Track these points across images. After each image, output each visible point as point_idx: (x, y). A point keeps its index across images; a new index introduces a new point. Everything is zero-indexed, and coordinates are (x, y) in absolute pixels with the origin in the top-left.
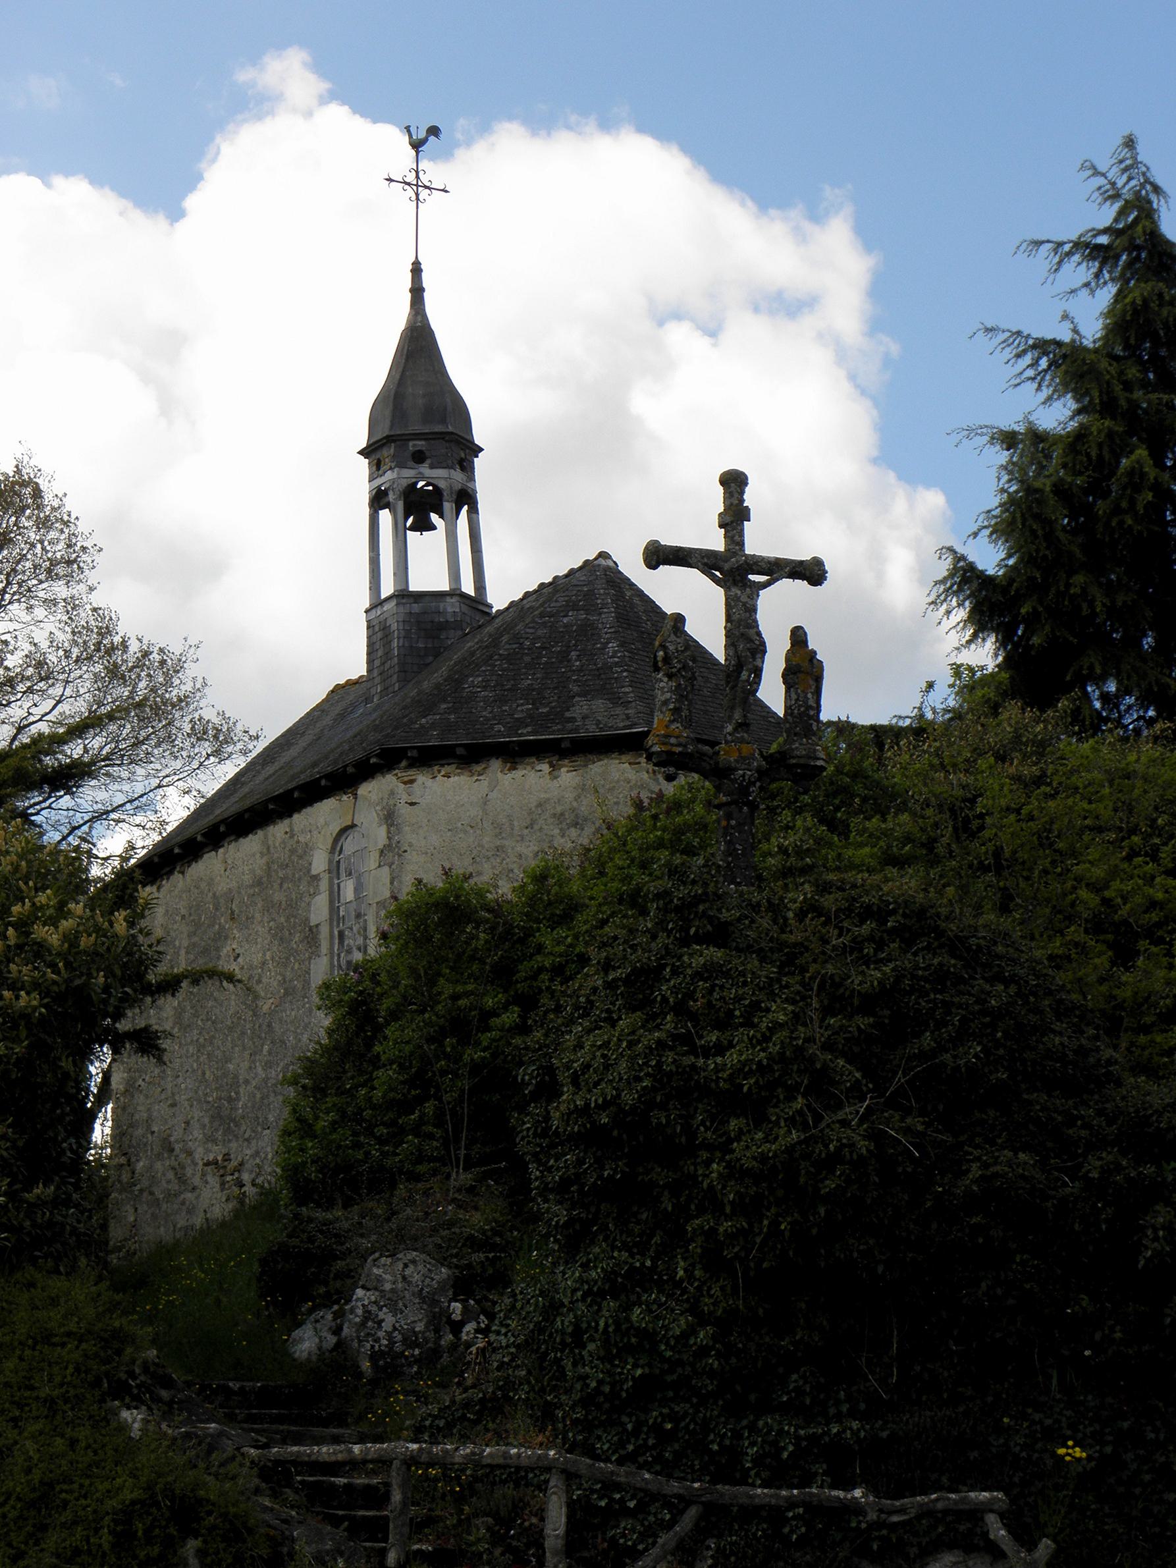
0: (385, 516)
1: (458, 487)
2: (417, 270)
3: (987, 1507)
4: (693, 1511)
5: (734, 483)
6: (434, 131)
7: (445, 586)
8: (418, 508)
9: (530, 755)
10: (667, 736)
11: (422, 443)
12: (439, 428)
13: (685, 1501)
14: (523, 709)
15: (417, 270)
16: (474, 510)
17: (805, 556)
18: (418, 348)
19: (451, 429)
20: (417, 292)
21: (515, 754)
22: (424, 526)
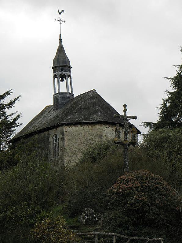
0: (56, 78)
1: (68, 75)
2: (60, 36)
3: (161, 240)
4: (129, 241)
5: (125, 106)
6: (63, 11)
7: (66, 92)
8: (63, 77)
9: (85, 124)
10: (117, 140)
11: (62, 67)
12: (65, 65)
13: (128, 239)
14: (83, 117)
15: (60, 36)
16: (71, 78)
17: (134, 116)
18: (61, 50)
19: (67, 65)
20: (60, 40)
21: (82, 124)
22: (62, 80)
